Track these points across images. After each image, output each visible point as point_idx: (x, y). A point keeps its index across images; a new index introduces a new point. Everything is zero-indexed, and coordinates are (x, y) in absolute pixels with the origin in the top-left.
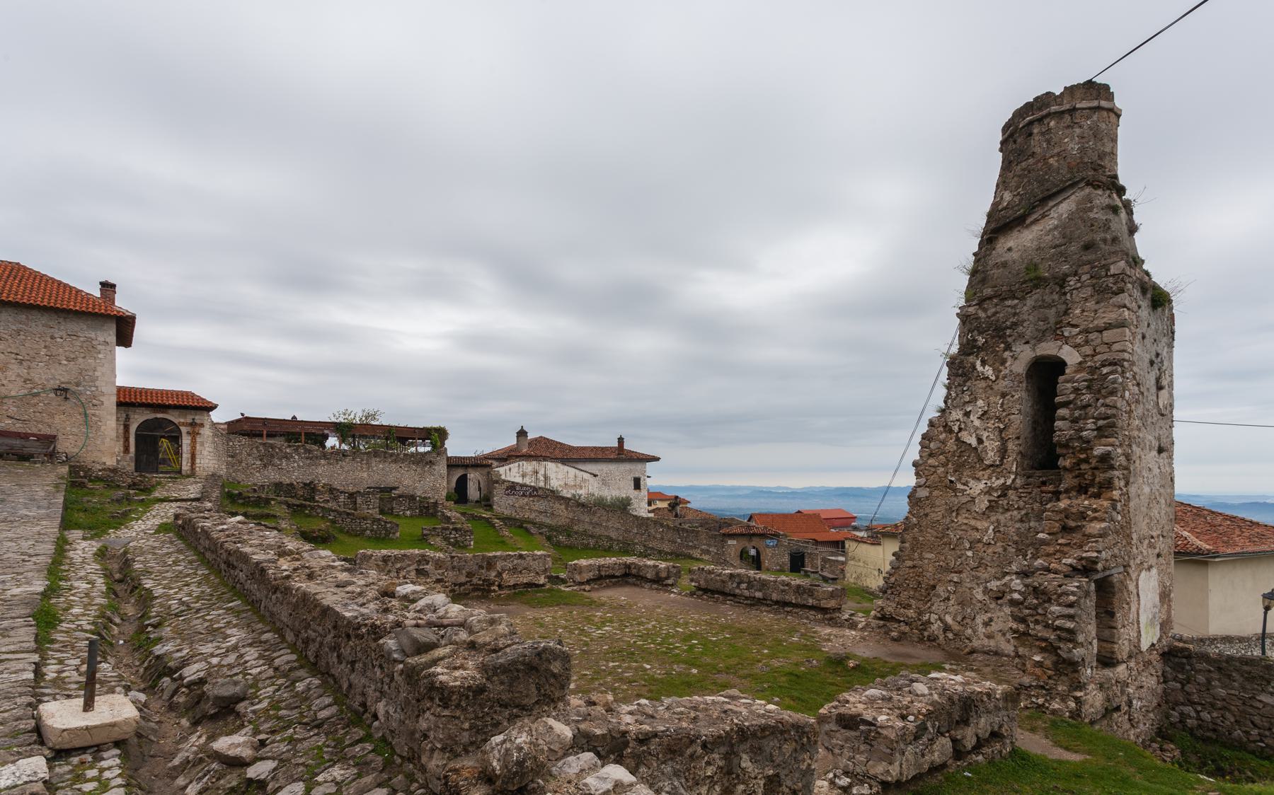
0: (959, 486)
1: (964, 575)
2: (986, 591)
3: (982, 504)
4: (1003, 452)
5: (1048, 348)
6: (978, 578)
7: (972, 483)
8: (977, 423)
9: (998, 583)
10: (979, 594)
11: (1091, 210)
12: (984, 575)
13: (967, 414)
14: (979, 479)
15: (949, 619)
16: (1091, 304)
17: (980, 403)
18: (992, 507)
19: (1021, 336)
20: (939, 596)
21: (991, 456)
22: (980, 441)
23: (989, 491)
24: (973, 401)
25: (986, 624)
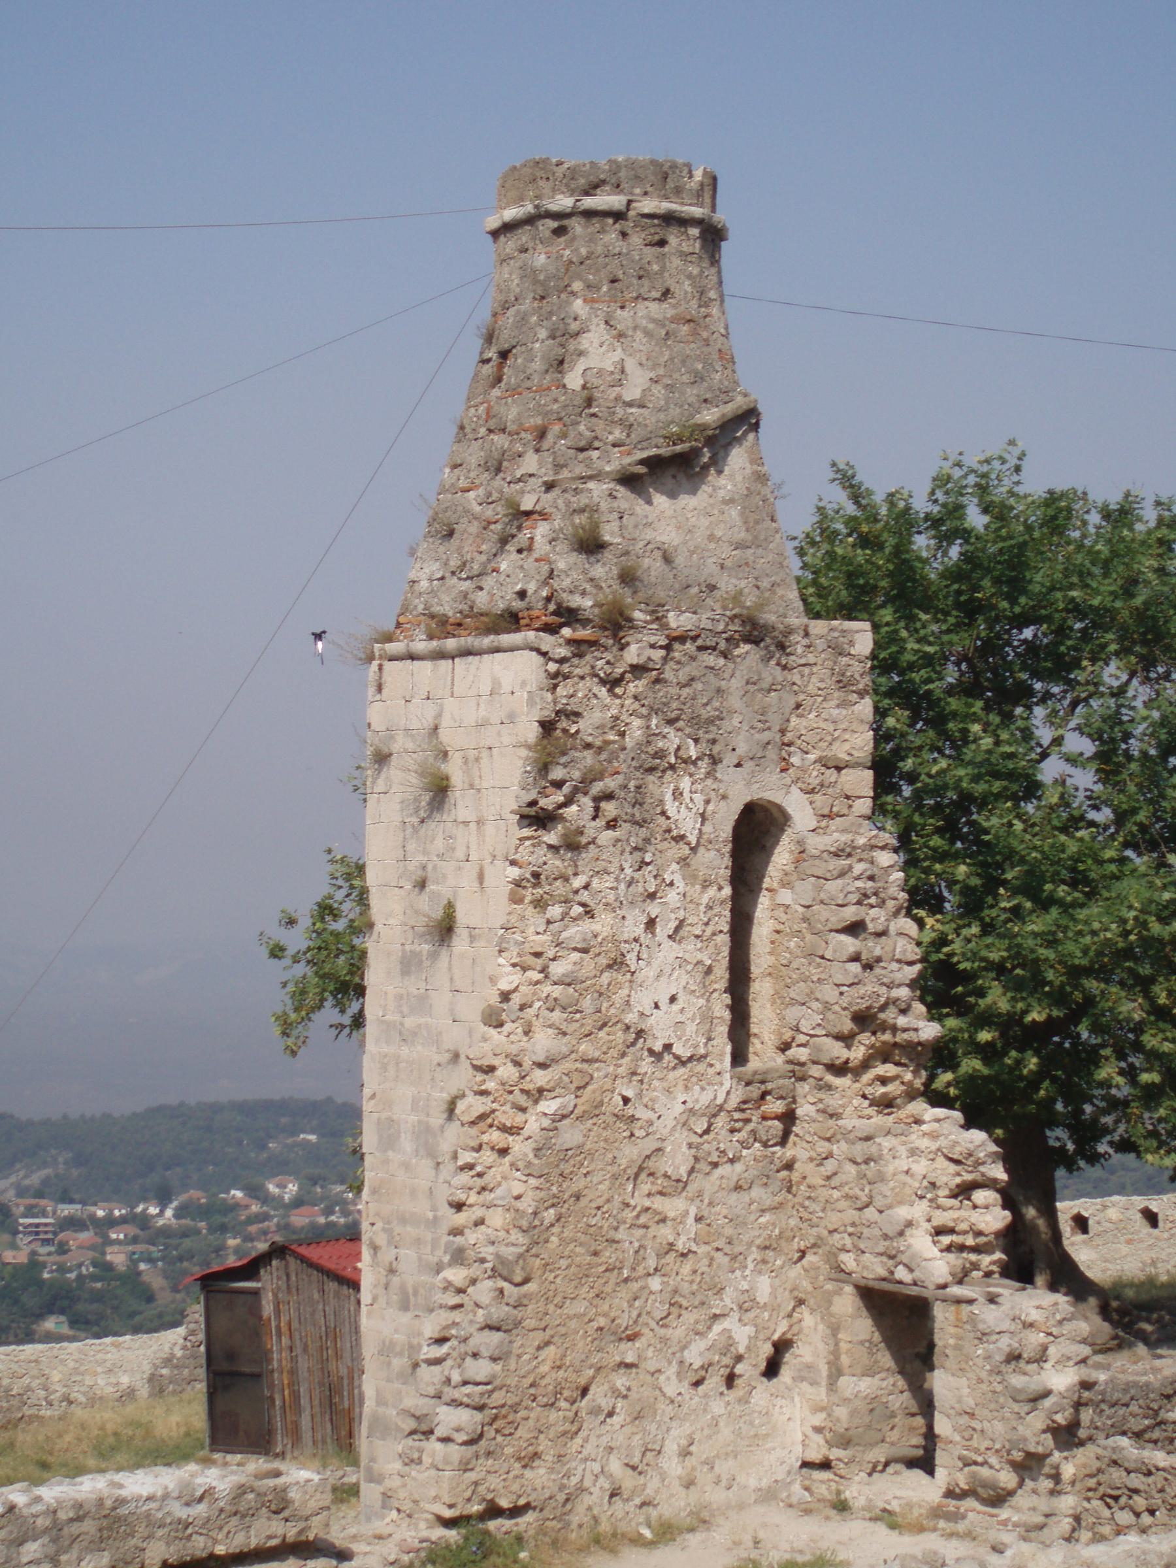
3: (677, 1161)
13: (651, 924)
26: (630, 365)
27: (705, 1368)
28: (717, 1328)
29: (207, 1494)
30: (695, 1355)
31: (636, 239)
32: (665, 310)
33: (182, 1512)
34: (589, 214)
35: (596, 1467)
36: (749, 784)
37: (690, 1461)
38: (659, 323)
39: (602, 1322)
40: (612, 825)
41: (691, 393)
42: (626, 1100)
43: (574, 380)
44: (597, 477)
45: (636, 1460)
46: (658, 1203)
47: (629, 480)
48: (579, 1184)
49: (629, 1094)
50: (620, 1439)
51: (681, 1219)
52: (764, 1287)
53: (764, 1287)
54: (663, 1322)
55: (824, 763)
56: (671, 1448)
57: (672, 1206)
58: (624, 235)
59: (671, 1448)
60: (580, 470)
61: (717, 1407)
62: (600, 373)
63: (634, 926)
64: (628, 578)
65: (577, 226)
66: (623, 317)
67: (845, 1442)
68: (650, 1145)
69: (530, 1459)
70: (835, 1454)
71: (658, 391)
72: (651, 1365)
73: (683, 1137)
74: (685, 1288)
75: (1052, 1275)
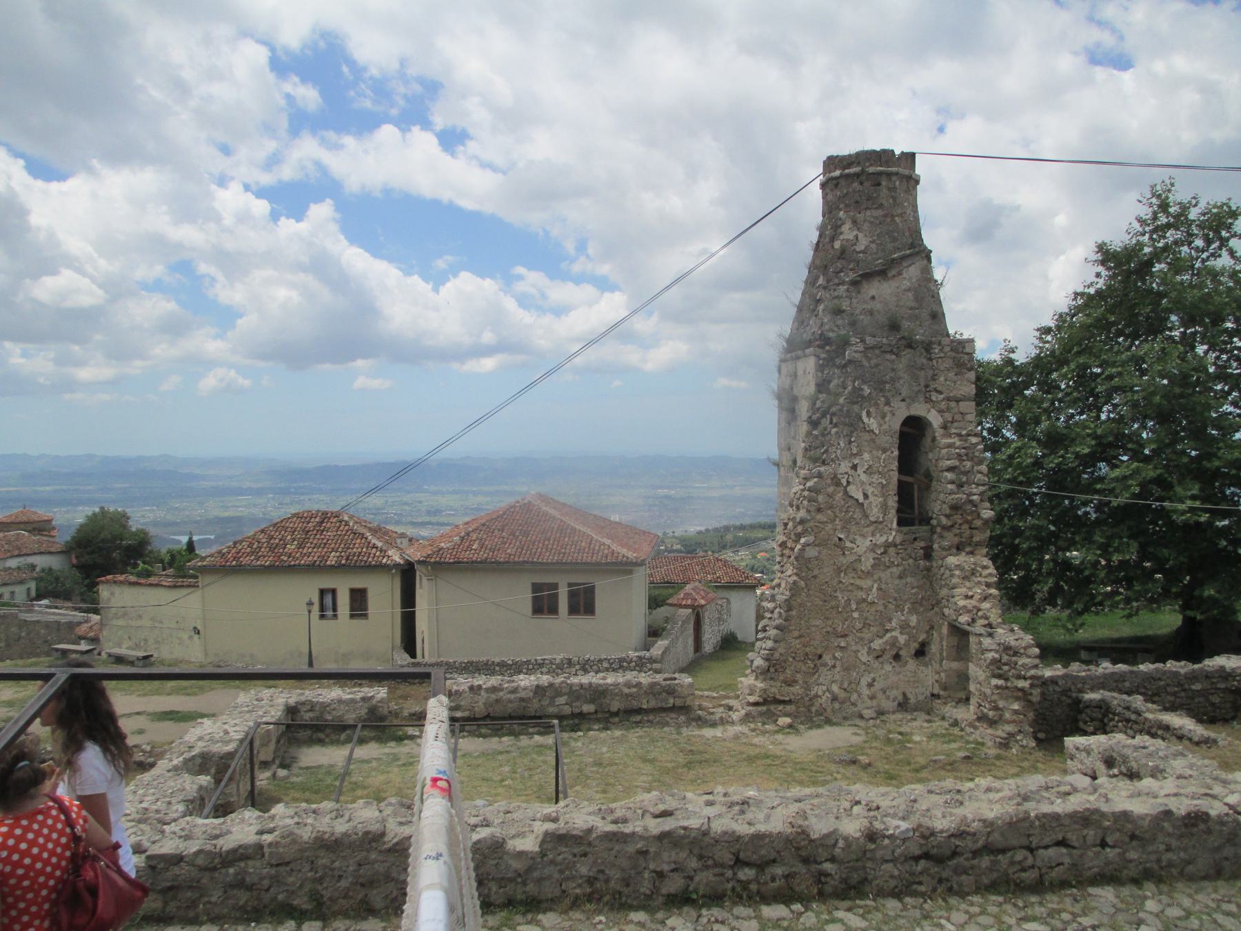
0: (848, 544)
1: (849, 639)
3: (867, 563)
4: (884, 508)
5: (919, 409)
6: (862, 639)
7: (859, 540)
8: (863, 477)
9: (881, 641)
12: (867, 635)
13: (854, 467)
14: (863, 536)
16: (951, 375)
17: (866, 456)
20: (825, 665)
21: (875, 513)
22: (866, 496)
24: (859, 454)
25: (870, 685)
26: (860, 236)
27: (883, 651)
28: (888, 635)
29: (639, 685)
30: (877, 644)
31: (867, 184)
32: (880, 212)
33: (626, 691)
34: (848, 176)
35: (824, 688)
36: (908, 408)
37: (873, 689)
38: (876, 218)
39: (829, 629)
40: (836, 425)
41: (890, 246)
42: (840, 539)
43: (837, 245)
44: (843, 283)
45: (845, 686)
46: (858, 582)
47: (855, 283)
48: (816, 572)
49: (842, 536)
50: (837, 677)
51: (871, 589)
52: (913, 620)
53: (913, 620)
54: (860, 631)
55: (948, 399)
56: (864, 682)
57: (866, 583)
58: (861, 183)
59: (864, 682)
60: (836, 281)
61: (888, 668)
62: (848, 240)
63: (844, 467)
64: (853, 324)
65: (842, 182)
66: (860, 217)
67: (945, 689)
68: (853, 558)
69: (790, 683)
70: (942, 693)
71: (873, 246)
72: (854, 648)
73: (871, 556)
74: (872, 618)
75: (95, 740)
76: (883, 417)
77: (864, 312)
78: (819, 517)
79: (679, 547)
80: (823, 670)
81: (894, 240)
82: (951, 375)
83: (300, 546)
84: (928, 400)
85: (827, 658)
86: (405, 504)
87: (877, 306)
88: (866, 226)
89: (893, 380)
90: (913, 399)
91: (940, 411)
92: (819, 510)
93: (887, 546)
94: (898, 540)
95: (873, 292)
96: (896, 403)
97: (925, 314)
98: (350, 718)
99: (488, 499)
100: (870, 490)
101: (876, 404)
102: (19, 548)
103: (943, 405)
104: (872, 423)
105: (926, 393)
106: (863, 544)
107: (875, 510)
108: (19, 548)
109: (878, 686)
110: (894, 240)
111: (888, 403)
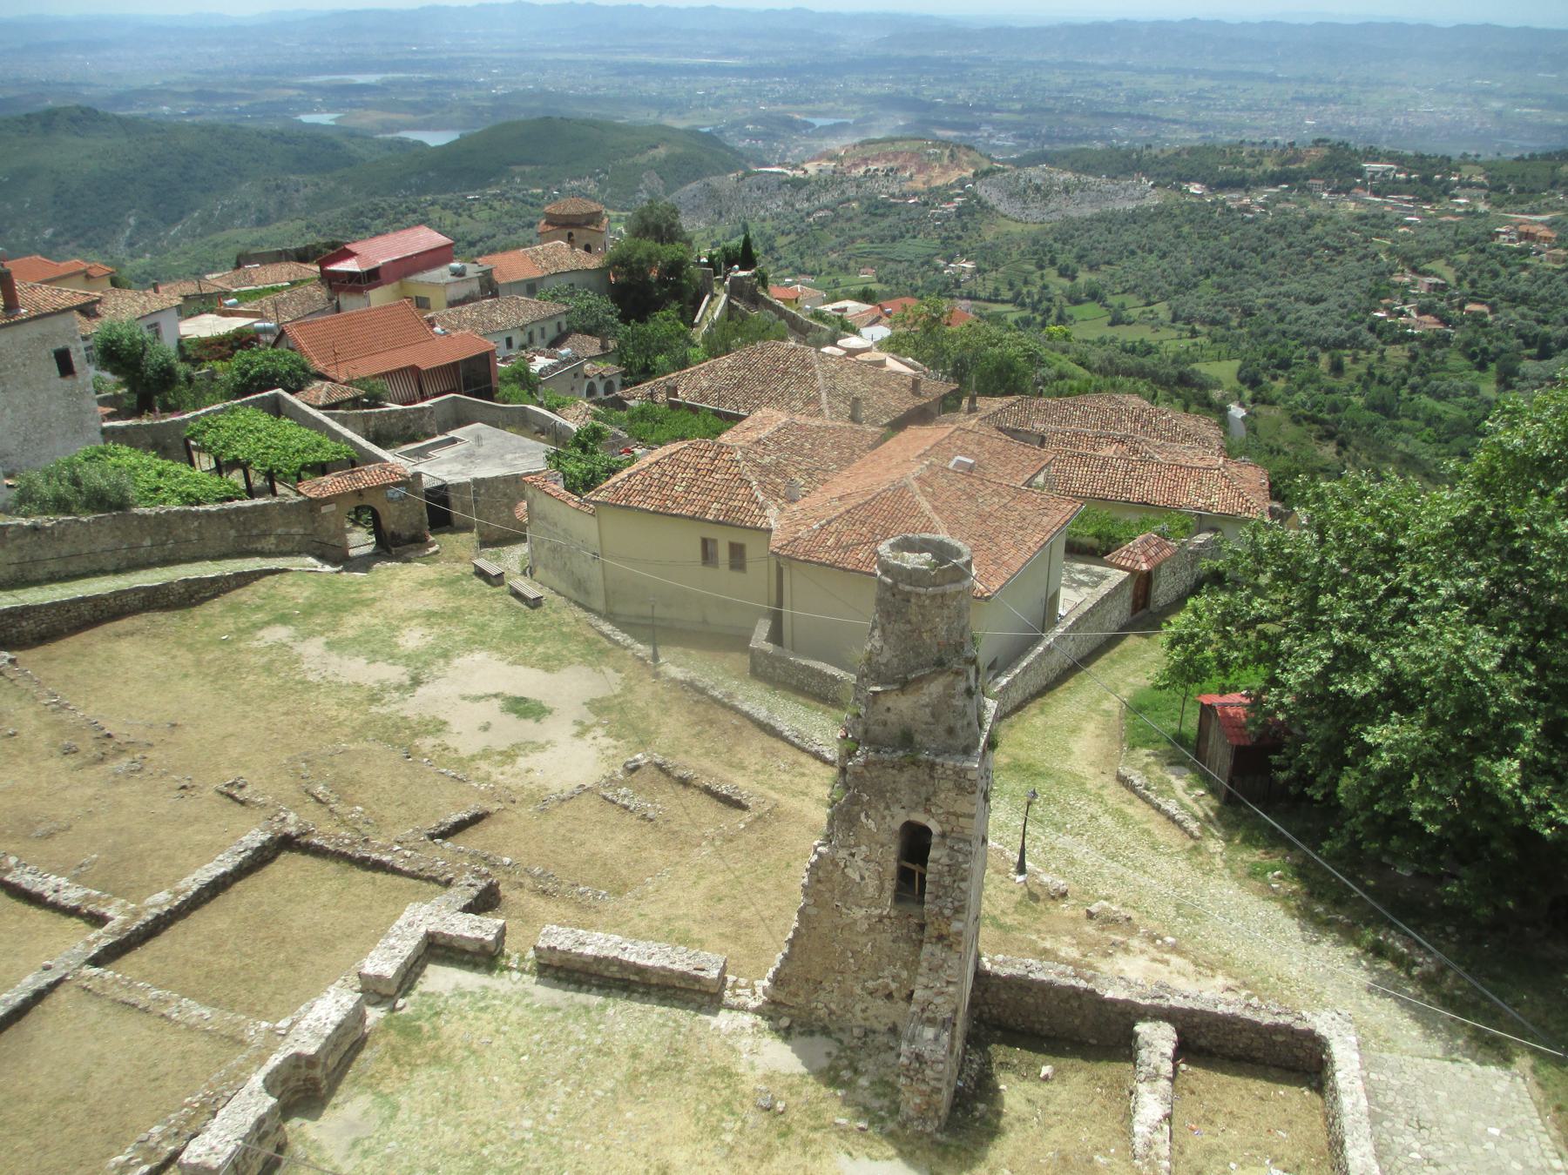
2: (863, 988)
4: (881, 889)
5: (919, 817)
7: (855, 909)
8: (861, 863)
10: (858, 990)
11: (953, 696)
12: (862, 975)
13: (853, 855)
15: (833, 1006)
16: (952, 794)
17: (863, 848)
18: (871, 929)
19: (898, 801)
21: (871, 891)
22: (862, 878)
23: (868, 917)
24: (857, 845)
25: (864, 1011)
30: (870, 984)
32: (908, 627)
56: (859, 1007)
57: (862, 940)
76: (884, 818)
77: (876, 722)
78: (819, 886)
79: (1481, 178)
80: (822, 994)
81: (918, 655)
82: (952, 794)
83: (687, 491)
84: (927, 811)
85: (826, 984)
86: (1099, 85)
87: (892, 717)
88: (892, 640)
89: (894, 790)
90: (913, 809)
91: (940, 822)
92: (819, 881)
93: (881, 919)
94: (893, 914)
95: (890, 704)
96: (896, 809)
97: (940, 730)
98: (469, 948)
99: (1215, 83)
100: (867, 874)
101: (876, 808)
102: (556, 265)
103: (942, 818)
104: (871, 824)
105: (926, 804)
106: (859, 913)
107: (871, 890)
108: (556, 265)
109: (870, 1013)
110: (918, 655)
111: (888, 807)
